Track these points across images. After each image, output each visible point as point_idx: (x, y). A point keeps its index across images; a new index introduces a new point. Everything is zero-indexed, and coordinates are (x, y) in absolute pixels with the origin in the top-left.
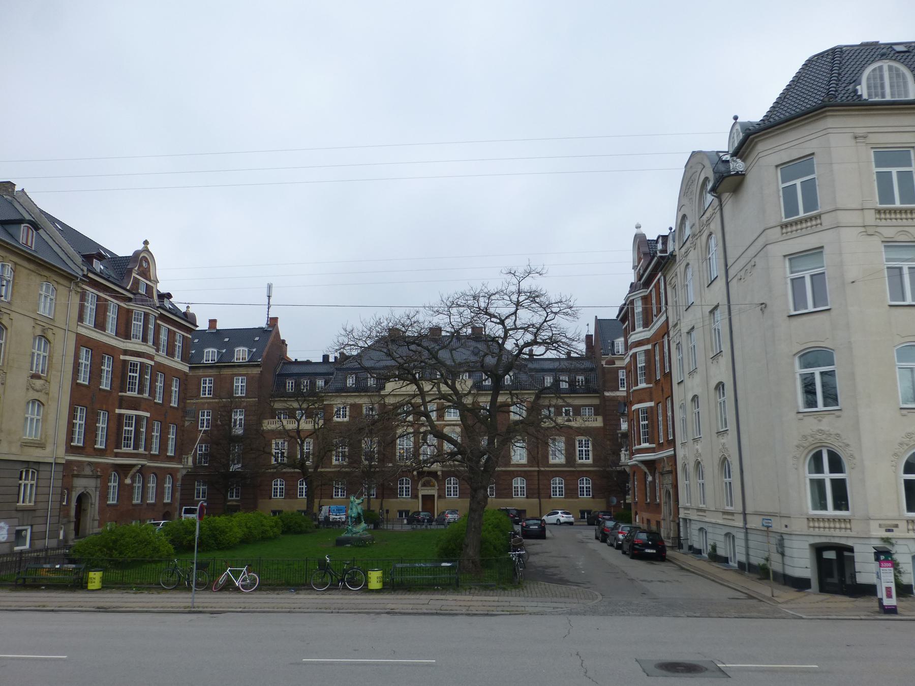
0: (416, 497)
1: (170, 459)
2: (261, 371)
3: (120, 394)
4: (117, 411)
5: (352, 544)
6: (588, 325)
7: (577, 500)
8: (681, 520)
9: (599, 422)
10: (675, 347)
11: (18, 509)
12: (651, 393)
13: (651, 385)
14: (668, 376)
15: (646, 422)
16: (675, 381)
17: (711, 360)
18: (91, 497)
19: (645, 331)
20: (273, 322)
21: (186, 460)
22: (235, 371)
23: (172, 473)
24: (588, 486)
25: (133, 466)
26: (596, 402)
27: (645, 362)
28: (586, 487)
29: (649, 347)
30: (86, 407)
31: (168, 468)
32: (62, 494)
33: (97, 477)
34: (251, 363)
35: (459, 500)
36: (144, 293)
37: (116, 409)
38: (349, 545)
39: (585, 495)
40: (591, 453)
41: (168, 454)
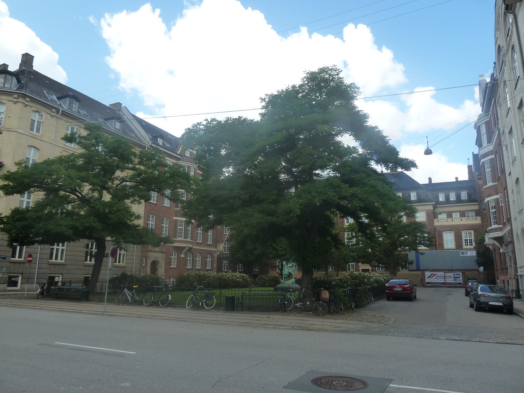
1: (209, 245)
3: (176, 209)
4: (175, 218)
8: (519, 277)
10: (505, 149)
11: (115, 266)
12: (496, 189)
13: (496, 183)
14: (503, 171)
16: (507, 173)
17: (522, 145)
18: (160, 263)
19: (489, 146)
23: (211, 253)
25: (184, 248)
27: (491, 168)
29: (493, 156)
30: (155, 215)
32: (141, 260)
33: (163, 252)
36: (189, 156)
37: (174, 217)
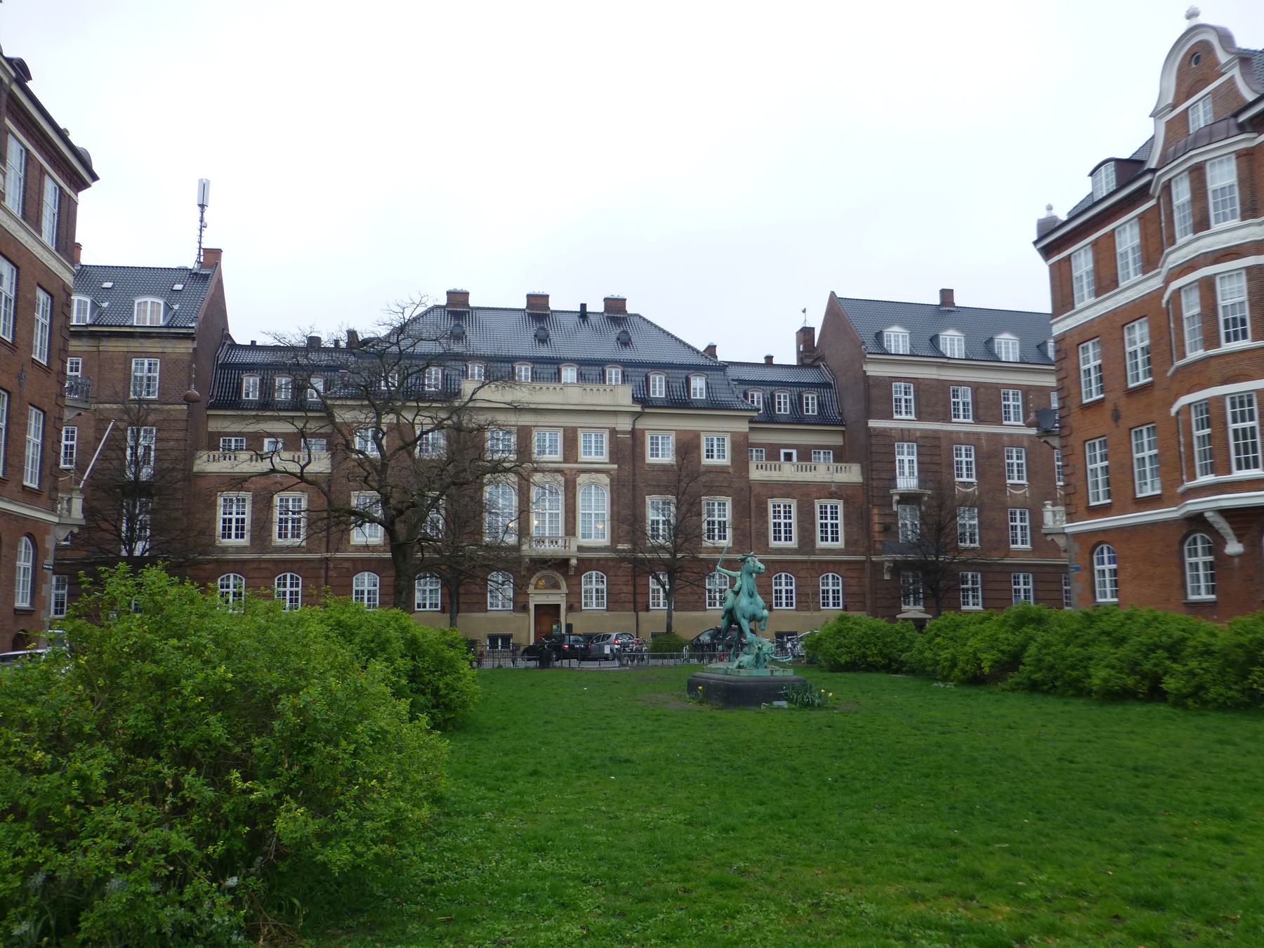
0: (525, 608)
2: (194, 349)
5: (790, 701)
6: (804, 311)
7: (816, 614)
9: (852, 474)
15: (1207, 431)
19: (1198, 239)
20: (212, 257)
21: (65, 505)
22: (134, 345)
24: (789, 588)
26: (837, 441)
28: (834, 591)
31: (25, 518)
34: (172, 330)
35: (608, 614)
38: (784, 704)
39: (831, 604)
40: (841, 529)
41: (25, 483)
